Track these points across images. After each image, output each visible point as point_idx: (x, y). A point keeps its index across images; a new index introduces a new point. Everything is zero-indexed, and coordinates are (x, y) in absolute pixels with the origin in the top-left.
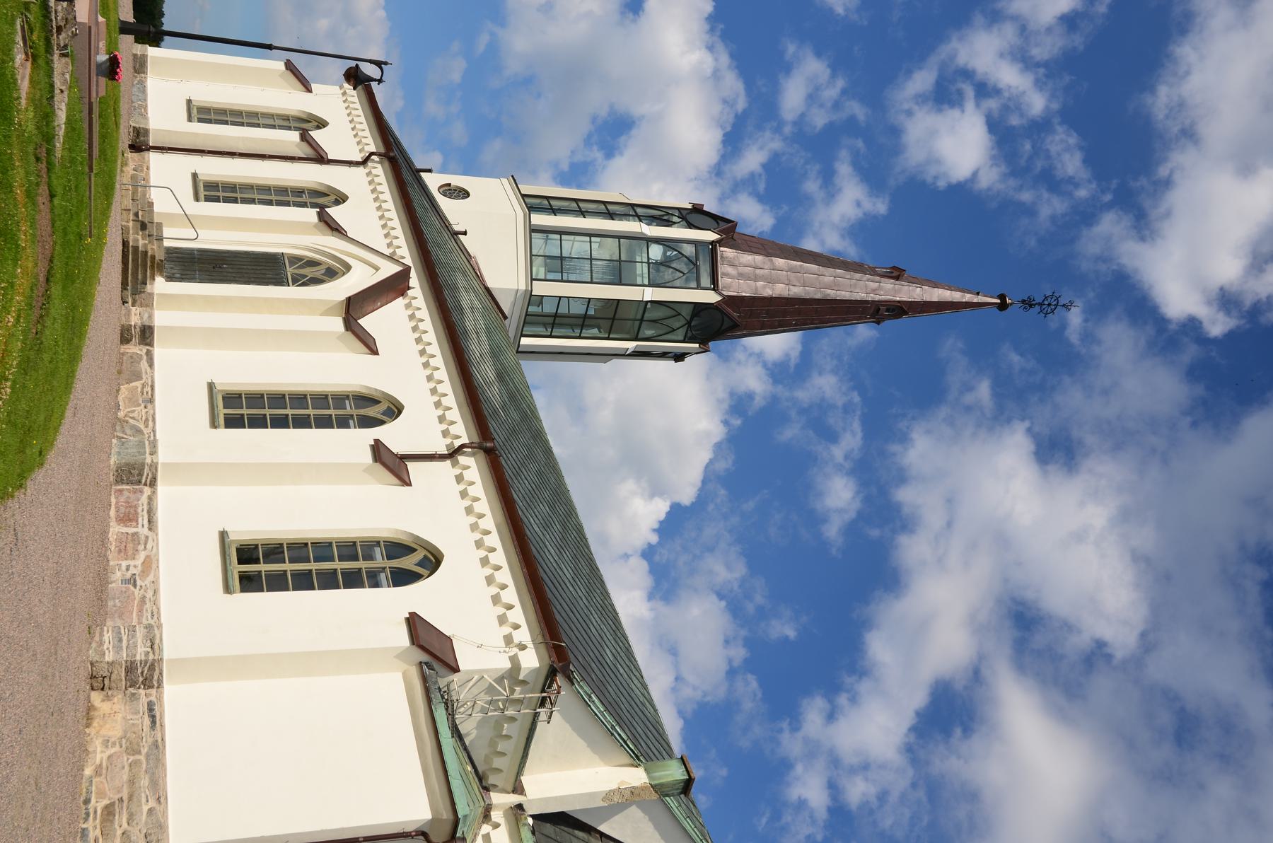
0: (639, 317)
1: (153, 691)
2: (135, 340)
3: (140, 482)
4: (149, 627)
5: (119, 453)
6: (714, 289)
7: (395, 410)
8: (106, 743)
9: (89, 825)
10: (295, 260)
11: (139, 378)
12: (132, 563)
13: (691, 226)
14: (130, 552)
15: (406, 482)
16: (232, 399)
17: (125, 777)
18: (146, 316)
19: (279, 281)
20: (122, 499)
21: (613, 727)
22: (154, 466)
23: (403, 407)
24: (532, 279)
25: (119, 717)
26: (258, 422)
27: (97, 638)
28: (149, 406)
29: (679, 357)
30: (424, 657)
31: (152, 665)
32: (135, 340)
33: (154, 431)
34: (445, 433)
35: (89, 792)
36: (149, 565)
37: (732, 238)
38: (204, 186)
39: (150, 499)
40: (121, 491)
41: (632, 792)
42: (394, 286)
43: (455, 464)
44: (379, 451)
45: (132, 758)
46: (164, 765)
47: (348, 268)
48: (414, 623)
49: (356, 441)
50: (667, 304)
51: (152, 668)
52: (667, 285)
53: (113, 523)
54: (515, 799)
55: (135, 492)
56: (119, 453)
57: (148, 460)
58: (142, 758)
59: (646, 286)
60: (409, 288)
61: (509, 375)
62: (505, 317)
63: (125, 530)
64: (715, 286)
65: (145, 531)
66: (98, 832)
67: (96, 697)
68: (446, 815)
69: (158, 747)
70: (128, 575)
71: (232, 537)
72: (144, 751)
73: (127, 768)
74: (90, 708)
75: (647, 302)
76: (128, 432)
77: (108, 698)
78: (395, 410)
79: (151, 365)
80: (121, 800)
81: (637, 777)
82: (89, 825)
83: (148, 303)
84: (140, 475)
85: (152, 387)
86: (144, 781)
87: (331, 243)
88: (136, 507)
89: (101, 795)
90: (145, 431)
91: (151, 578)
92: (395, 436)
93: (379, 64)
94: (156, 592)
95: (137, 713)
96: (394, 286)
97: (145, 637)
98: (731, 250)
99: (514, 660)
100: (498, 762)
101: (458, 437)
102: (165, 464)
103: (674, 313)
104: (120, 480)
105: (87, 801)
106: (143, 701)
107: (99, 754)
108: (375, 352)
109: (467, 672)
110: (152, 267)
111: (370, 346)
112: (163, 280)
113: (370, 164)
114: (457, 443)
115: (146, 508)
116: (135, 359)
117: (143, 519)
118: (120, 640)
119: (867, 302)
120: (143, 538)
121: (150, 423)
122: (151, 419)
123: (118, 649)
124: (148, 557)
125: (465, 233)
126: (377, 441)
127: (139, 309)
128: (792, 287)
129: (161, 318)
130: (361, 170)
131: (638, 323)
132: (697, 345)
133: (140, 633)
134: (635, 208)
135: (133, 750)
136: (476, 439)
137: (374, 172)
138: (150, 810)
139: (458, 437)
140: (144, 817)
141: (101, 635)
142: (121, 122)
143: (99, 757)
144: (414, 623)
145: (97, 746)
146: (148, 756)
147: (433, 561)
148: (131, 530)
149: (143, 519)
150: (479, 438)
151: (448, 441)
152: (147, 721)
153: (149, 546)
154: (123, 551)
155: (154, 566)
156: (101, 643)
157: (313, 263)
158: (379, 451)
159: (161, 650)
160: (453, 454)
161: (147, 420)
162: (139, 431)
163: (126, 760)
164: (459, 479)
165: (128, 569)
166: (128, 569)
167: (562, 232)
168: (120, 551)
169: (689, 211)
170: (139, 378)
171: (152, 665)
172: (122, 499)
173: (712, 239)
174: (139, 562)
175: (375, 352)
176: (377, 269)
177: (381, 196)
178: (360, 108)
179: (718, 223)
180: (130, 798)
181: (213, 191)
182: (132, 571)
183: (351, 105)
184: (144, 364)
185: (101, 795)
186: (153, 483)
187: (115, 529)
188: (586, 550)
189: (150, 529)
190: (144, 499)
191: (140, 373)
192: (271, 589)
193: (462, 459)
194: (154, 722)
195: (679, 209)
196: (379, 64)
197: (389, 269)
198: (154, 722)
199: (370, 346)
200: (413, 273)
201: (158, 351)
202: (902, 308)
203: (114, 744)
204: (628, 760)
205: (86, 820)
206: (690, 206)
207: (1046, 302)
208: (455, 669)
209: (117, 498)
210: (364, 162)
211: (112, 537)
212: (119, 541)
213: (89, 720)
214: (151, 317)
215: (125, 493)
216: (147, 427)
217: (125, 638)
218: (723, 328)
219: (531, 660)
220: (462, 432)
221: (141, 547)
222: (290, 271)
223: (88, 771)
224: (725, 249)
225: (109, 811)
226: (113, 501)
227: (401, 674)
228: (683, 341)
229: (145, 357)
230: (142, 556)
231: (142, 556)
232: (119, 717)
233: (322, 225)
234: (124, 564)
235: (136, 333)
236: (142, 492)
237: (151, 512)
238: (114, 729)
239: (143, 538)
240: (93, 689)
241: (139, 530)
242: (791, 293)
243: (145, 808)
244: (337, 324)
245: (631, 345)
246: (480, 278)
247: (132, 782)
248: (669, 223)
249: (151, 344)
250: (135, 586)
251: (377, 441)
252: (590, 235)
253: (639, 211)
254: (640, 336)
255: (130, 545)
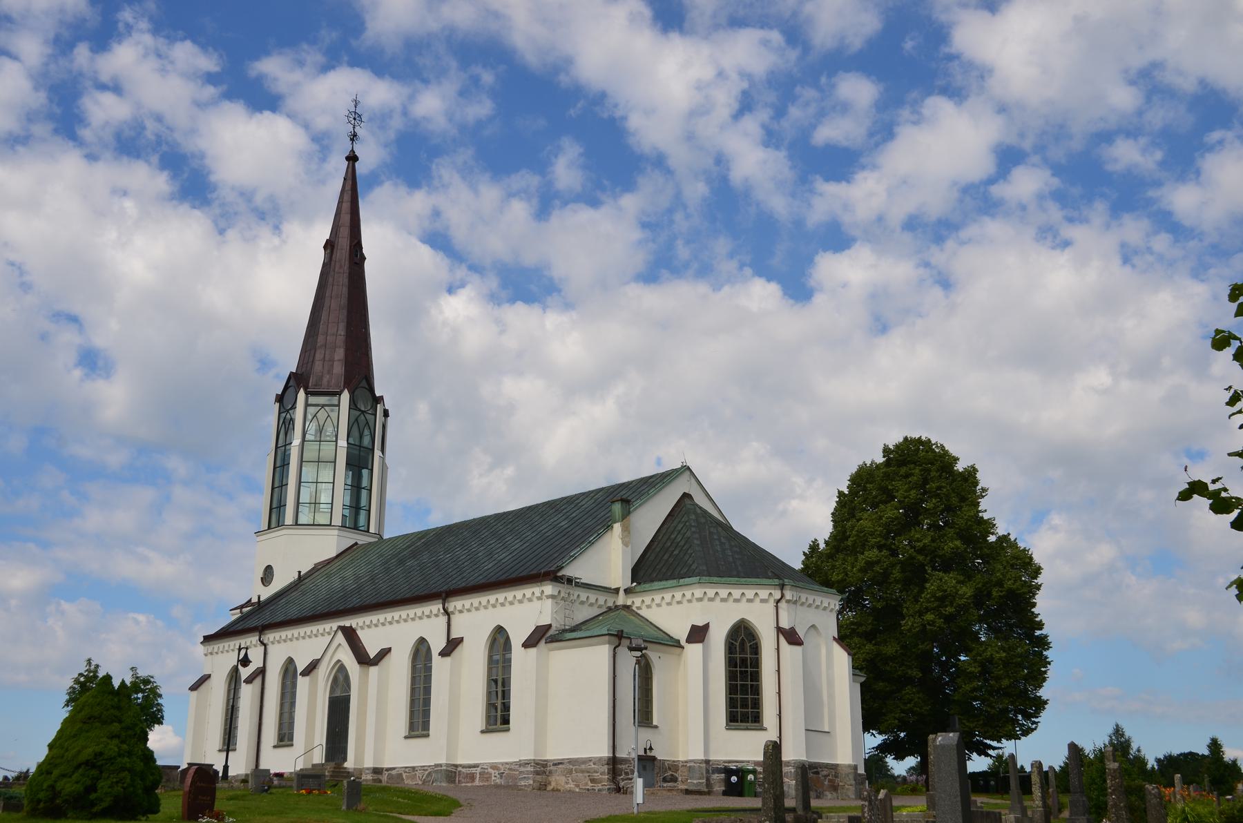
0: (358, 448)
1: (549, 763)
2: (380, 777)
3: (455, 772)
4: (520, 765)
5: (441, 782)
6: (340, 395)
7: (422, 641)
8: (567, 783)
9: (597, 788)
10: (332, 690)
11: (401, 774)
12: (493, 775)
13: (294, 407)
14: (488, 776)
15: (461, 640)
16: (412, 726)
17: (581, 775)
18: (367, 771)
19: (347, 700)
20: (463, 780)
21: (590, 542)
22: (447, 765)
23: (421, 637)
24: (330, 525)
25: (558, 778)
26: (426, 714)
27: (523, 787)
28: (416, 769)
29: (386, 414)
30: (543, 641)
31: (536, 764)
32: (380, 777)
33: (429, 766)
34: (436, 616)
35: (585, 789)
36: (494, 767)
37: (301, 375)
38: (281, 741)
39: (463, 767)
40: (459, 781)
41: (625, 531)
42: (351, 636)
43: (453, 613)
44: (445, 653)
45: (574, 772)
46: (578, 758)
47: (339, 661)
48: (529, 643)
49: (440, 667)
50: (350, 426)
51: (537, 764)
52: (336, 424)
53: (474, 784)
54: (621, 592)
55: (459, 775)
56: (441, 782)
57: (445, 768)
58: (574, 768)
59: (337, 444)
60: (351, 627)
61: (399, 553)
62: (356, 544)
63: (478, 779)
64: (339, 394)
65: (479, 769)
66: (599, 785)
67: (549, 788)
68: (607, 638)
69: (571, 761)
70: (499, 776)
71: (276, 744)
72: (571, 767)
73: (578, 774)
74: (553, 790)
75: (348, 443)
76: (429, 779)
77: (550, 783)
78: (422, 641)
79: (394, 769)
80: (589, 776)
81: (617, 527)
82: (597, 788)
83: (361, 771)
84: (451, 772)
85: (406, 768)
86: (583, 767)
87: (323, 672)
88: (467, 774)
89: (587, 784)
90: (429, 770)
91: (500, 766)
92: (437, 643)
93: (240, 649)
94: (507, 763)
95: (556, 770)
96: (351, 636)
97: (524, 767)
98: (311, 378)
99: (548, 597)
100: (601, 602)
101: (439, 609)
102: (447, 759)
103: (356, 423)
104: (454, 782)
105: (588, 790)
106: (552, 768)
107: (571, 786)
108: (390, 650)
109: (552, 620)
110: (337, 768)
111: (385, 653)
112: (346, 763)
113: (265, 642)
114: (442, 611)
115: (468, 769)
116: (390, 777)
117: (473, 770)
118: (525, 777)
119: (350, 274)
120: (482, 770)
121: (425, 768)
122: (423, 768)
123: (528, 778)
124: (491, 768)
125: (300, 572)
126: (440, 654)
127: (363, 775)
128: (339, 333)
129: (369, 763)
130: (270, 648)
131: (362, 449)
132: (378, 405)
133: (522, 769)
134: (279, 446)
135: (570, 772)
136: (441, 601)
137: (271, 639)
138: (594, 764)
139: (439, 609)
140: (596, 766)
141: (522, 786)
142: (181, 809)
143: (572, 786)
144: (529, 643)
145: (567, 787)
146: (573, 766)
147: (500, 630)
148: (478, 776)
149: (473, 770)
150: (439, 599)
151: (441, 615)
152: (560, 766)
153: (486, 767)
154: (488, 779)
155: (495, 765)
156: (525, 785)
157: (335, 680)
158: (445, 653)
159: (530, 760)
160: (447, 612)
161: (424, 770)
162: (430, 773)
163: (574, 774)
164: (461, 612)
165: (495, 776)
166: (495, 776)
167: (298, 504)
168: (488, 781)
169: (282, 407)
170: (401, 774)
171: (536, 764)
172: (463, 780)
173: (304, 394)
174: (493, 771)
175: (390, 650)
176: (340, 645)
177: (289, 637)
178: (223, 644)
179: (290, 387)
180: (588, 772)
181: (285, 738)
182: (497, 774)
183: (221, 650)
184: (394, 772)
185: (587, 784)
186: (456, 766)
187: (477, 783)
188: (510, 517)
189: (478, 767)
190: (464, 770)
191: (398, 774)
192: (509, 711)
193: (451, 609)
194: (561, 763)
195: (279, 414)
196: (240, 649)
197: (340, 638)
198: (561, 763)
199: (385, 653)
200: (342, 624)
201: (386, 765)
202: (355, 245)
203: (568, 780)
204: (609, 533)
205: (595, 790)
206: (277, 404)
207: (353, 122)
208: (550, 626)
209: (462, 783)
210: (265, 645)
211: (481, 784)
212: (482, 781)
213: (558, 790)
214: (368, 769)
215: (460, 779)
216: (427, 770)
217: (524, 776)
218: (367, 387)
219: (549, 589)
220: (436, 607)
221: (486, 771)
222: (338, 693)
223: (577, 790)
224: (311, 381)
225: (593, 781)
226: (463, 784)
227: (552, 653)
228: (375, 415)
229: (390, 772)
230: (490, 770)
231: (490, 770)
232: (558, 778)
233: (313, 674)
234: (493, 778)
235: (376, 777)
236: (460, 772)
237: (470, 766)
238: (562, 779)
239: (482, 770)
240: (545, 790)
241: (478, 772)
242: (343, 333)
243: (593, 766)
244: (373, 670)
245: (377, 453)
246: (329, 562)
247: (582, 771)
248: (292, 420)
249: (382, 769)
250: (503, 773)
251: (440, 654)
252: (300, 482)
253: (281, 443)
254: (370, 447)
255: (485, 775)
